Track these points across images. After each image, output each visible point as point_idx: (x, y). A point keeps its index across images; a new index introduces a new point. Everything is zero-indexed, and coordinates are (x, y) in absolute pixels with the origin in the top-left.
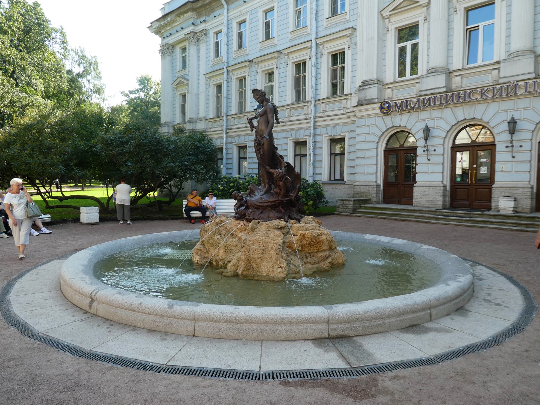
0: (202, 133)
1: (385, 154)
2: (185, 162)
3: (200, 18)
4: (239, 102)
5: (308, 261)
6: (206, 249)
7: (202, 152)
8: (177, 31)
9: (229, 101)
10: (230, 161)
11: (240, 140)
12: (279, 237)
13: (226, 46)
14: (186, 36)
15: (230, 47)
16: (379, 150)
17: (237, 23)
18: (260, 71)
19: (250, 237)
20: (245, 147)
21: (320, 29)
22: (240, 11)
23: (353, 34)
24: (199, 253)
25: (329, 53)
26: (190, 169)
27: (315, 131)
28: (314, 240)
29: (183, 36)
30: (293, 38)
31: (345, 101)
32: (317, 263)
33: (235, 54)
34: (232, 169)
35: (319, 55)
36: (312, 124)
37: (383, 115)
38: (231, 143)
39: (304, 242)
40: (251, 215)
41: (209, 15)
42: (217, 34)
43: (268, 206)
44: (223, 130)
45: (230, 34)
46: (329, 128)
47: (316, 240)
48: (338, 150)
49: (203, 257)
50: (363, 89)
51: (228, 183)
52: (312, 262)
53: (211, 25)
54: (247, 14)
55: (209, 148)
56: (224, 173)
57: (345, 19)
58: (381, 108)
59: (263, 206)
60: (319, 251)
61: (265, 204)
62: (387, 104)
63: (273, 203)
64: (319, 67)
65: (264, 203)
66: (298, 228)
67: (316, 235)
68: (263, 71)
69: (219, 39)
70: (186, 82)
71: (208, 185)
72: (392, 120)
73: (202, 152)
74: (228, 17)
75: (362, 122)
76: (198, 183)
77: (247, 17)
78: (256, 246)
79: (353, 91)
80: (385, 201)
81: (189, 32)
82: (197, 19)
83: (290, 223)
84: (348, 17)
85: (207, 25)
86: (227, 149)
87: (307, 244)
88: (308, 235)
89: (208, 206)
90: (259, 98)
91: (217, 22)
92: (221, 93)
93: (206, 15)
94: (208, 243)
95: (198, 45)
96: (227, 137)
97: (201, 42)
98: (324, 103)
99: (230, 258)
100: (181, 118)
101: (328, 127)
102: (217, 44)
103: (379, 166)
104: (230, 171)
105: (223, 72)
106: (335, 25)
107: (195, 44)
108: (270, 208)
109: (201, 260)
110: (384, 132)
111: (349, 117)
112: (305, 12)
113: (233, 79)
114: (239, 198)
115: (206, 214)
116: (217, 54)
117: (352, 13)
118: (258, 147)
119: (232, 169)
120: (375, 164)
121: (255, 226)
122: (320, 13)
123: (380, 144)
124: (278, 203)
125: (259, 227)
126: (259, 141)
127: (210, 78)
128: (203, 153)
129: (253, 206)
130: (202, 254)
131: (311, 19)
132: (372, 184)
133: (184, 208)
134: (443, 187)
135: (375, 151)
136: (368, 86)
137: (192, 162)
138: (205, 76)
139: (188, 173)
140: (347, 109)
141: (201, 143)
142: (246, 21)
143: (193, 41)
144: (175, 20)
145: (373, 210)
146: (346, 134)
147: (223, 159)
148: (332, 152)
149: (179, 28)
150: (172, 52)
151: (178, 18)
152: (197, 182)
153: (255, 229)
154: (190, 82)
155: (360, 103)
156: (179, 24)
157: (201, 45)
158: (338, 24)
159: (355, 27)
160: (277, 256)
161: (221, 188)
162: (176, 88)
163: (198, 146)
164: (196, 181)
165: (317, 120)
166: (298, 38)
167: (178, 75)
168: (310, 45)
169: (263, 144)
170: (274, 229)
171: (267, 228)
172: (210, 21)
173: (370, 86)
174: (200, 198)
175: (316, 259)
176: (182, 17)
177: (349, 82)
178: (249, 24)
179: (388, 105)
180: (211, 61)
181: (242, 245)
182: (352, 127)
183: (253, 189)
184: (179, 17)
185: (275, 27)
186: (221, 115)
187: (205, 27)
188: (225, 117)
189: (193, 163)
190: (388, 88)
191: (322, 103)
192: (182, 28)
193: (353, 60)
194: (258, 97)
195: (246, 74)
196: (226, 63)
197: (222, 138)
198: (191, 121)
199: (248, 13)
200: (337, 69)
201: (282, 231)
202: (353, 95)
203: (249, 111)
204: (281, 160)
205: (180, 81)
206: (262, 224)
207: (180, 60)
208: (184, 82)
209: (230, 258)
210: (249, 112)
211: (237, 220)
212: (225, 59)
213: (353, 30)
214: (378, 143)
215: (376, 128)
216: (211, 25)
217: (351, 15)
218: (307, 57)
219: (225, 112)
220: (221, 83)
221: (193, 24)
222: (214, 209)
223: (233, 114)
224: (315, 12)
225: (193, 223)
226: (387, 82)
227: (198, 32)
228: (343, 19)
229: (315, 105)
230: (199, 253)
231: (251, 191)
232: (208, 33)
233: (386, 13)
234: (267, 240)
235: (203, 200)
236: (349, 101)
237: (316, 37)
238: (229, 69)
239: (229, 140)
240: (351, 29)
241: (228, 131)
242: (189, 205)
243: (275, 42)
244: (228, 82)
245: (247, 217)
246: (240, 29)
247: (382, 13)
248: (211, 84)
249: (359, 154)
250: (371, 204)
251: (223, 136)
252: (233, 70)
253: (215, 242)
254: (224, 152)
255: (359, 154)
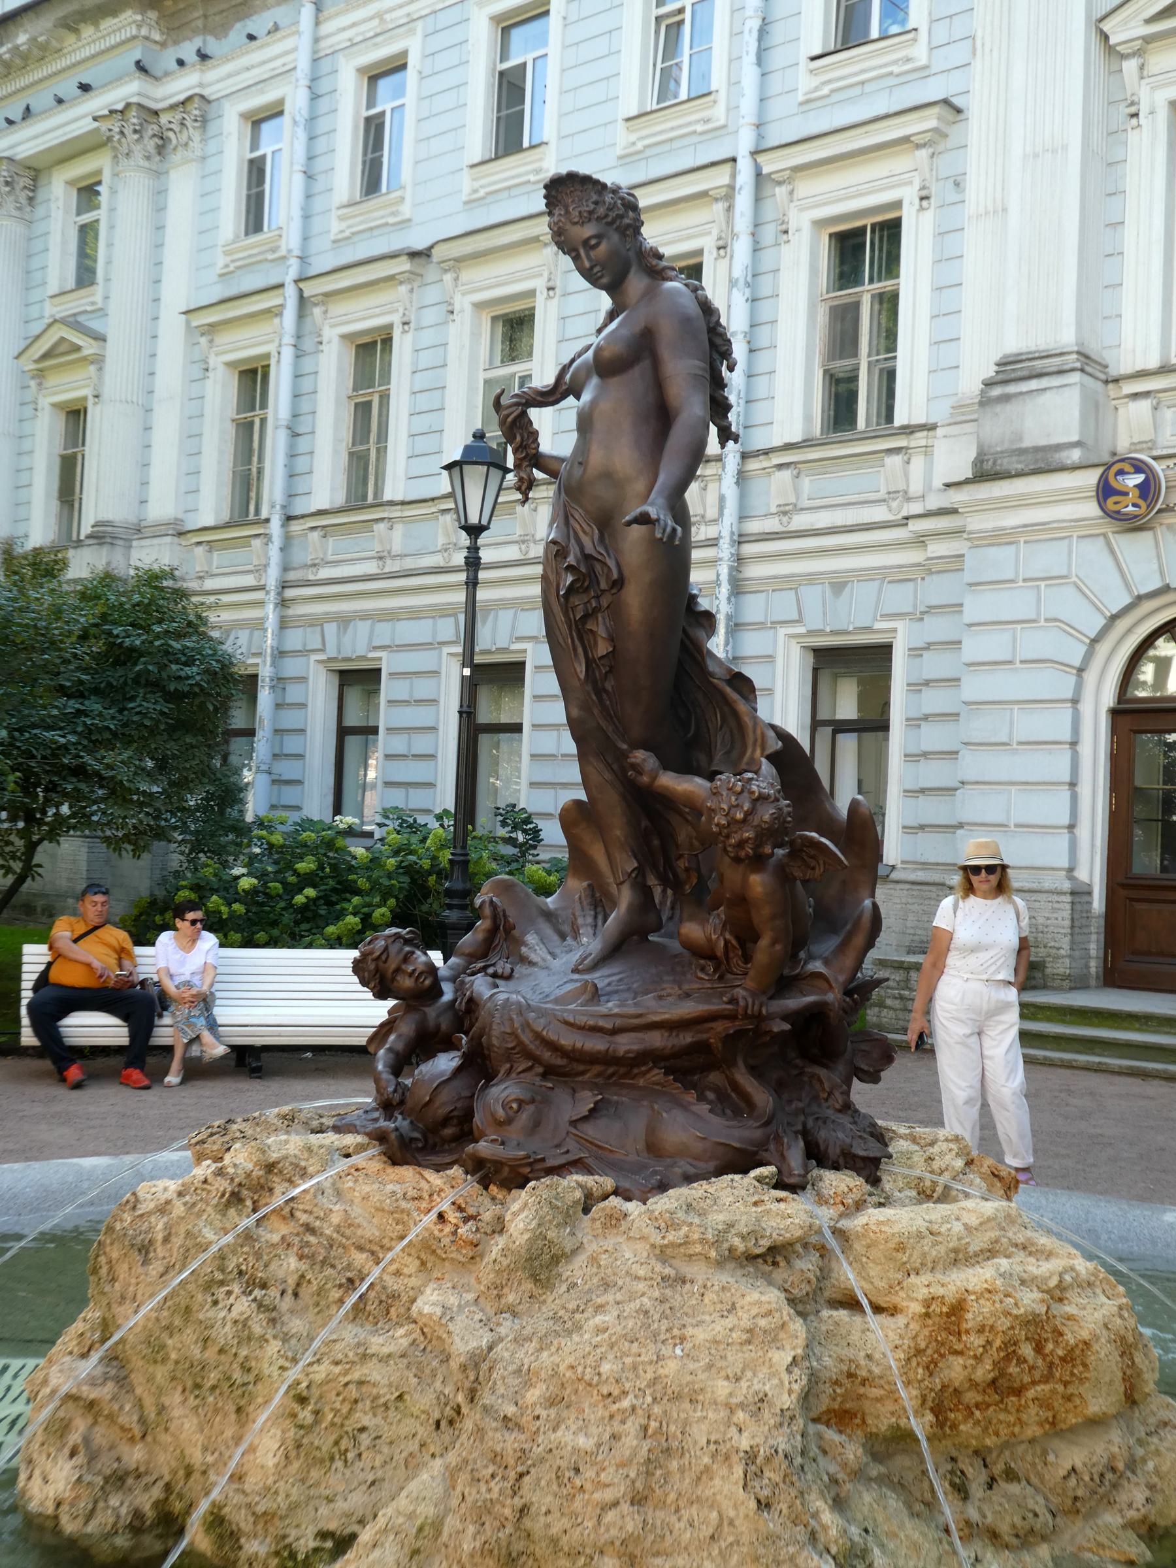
0: (152, 579)
1: (1114, 730)
2: (49, 728)
3: (176, 43)
4: (351, 454)
5: (973, 1515)
6: (139, 1404)
7: (149, 684)
8: (60, 101)
9: (303, 444)
10: (292, 744)
11: (347, 639)
12: (773, 1338)
13: (298, 179)
14: (104, 126)
15: (318, 186)
16: (1086, 707)
17: (361, 71)
18: (463, 303)
19: (520, 1340)
20: (373, 676)
21: (777, 108)
22: (379, 15)
23: (945, 136)
24: (80, 1425)
25: (819, 224)
26: (80, 771)
27: (737, 608)
28: (1027, 1350)
29: (88, 125)
30: (639, 146)
31: (896, 460)
32: (1044, 1538)
33: (341, 219)
34: (299, 782)
35: (769, 233)
36: (724, 571)
37: (1108, 527)
38: (305, 652)
39: (955, 1370)
40: (514, 1132)
41: (221, 31)
42: (257, 120)
43: (647, 1057)
44: (262, 588)
45: (322, 125)
46: (812, 596)
47: (1039, 1349)
48: (847, 708)
49: (106, 1464)
50: (1006, 398)
51: (284, 855)
52: (1004, 1528)
53: (229, 76)
54: (412, 32)
55: (189, 663)
56: (254, 806)
57: (908, 60)
58: (1106, 491)
59: (606, 1059)
60: (1055, 1428)
61: (626, 1044)
62: (1138, 470)
63: (687, 1038)
64: (765, 290)
65: (614, 1032)
66: (901, 1248)
67: (1030, 1300)
68: (479, 306)
69: (265, 149)
70: (89, 348)
71: (176, 860)
72: (1159, 557)
73: (149, 684)
74: (316, 40)
75: (1000, 562)
76: (118, 850)
77: (414, 46)
78: (584, 1429)
79: (939, 414)
80: (1112, 978)
81: (120, 107)
82: (163, 45)
83: (821, 1200)
84: (920, 52)
85: (212, 75)
86: (280, 683)
87: (973, 1384)
88: (986, 1307)
89: (170, 987)
90: (599, 237)
91: (264, 63)
92: (264, 405)
93: (206, 30)
94: (156, 1352)
95: (158, 174)
96: (283, 624)
97: (176, 158)
98: (786, 465)
99: (341, 1505)
100: (53, 521)
101: (803, 590)
102: (256, 171)
103: (1084, 790)
104: (289, 795)
105: (277, 301)
106: (857, 91)
107: (146, 164)
108: (657, 1075)
109: (83, 1505)
110: (1114, 618)
111: (920, 540)
112: (703, 32)
113: (325, 339)
114: (407, 983)
115: (157, 1031)
116: (254, 217)
117: (941, 36)
118: (576, 600)
119: (299, 782)
120: (1067, 778)
121: (561, 1237)
122: (778, 33)
123: (1091, 677)
124: (731, 1040)
125: (592, 1247)
126: (587, 557)
127: (212, 329)
128: (156, 686)
129: (529, 1055)
130: (102, 1435)
131: (734, 60)
132: (1047, 885)
133: (27, 995)
134: (1073, 893)
135: (1067, 714)
136: (1034, 384)
137: (89, 731)
138: (188, 323)
139: (65, 795)
140: (908, 499)
141: (147, 629)
142: (403, 67)
143: (137, 148)
144: (54, 43)
145: (1063, 1022)
146: (899, 625)
147: (260, 734)
148: (823, 715)
149: (67, 87)
150: (31, 199)
151: (71, 39)
152: (114, 844)
153: (556, 1260)
154: (113, 350)
155: (988, 466)
156: (74, 65)
157: (173, 175)
158: (868, 88)
159: (956, 101)
160: (771, 1523)
161: (246, 883)
162: (40, 374)
163: (132, 649)
164: (107, 840)
165: (749, 549)
166: (666, 147)
167: (51, 310)
168: (726, 180)
169: (619, 583)
170: (720, 1264)
171: (663, 1254)
172: (227, 59)
173: (1044, 382)
174: (120, 936)
175: (1038, 1504)
176: (88, 31)
177: (922, 366)
178: (422, 77)
179: (1140, 478)
180: (220, 250)
181: (442, 1400)
182: (938, 590)
183: (513, 915)
184: (76, 31)
185: (551, 94)
186: (257, 511)
187: (201, 85)
188: (275, 527)
189: (95, 740)
190: (1136, 396)
191: (780, 467)
192: (85, 88)
193: (945, 259)
194: (588, 231)
195: (396, 318)
196: (294, 264)
197: (258, 625)
198: (103, 536)
199: (420, 25)
200: (856, 306)
201: (780, 1275)
202: (940, 432)
203: (399, 497)
204: (742, 707)
205: (62, 339)
206: (615, 1220)
207: (64, 242)
208: (78, 348)
209: (341, 1505)
210: (403, 503)
211: (395, 1160)
212: (292, 241)
213: (949, 115)
214: (1081, 670)
215: (1070, 591)
216: (229, 76)
217: (934, 44)
218: (708, 243)
219: (279, 497)
220: (267, 356)
221: (140, 67)
222: (205, 1002)
223: (321, 513)
224: (755, 24)
225: (78, 1086)
226: (1125, 368)
227: (164, 110)
228: (895, 62)
229: (742, 477)
230: (80, 1425)
231: (493, 932)
232: (211, 116)
233: (1123, 30)
234: (670, 1368)
235: (139, 950)
236: (918, 462)
237: (757, 145)
238: (309, 289)
239: (294, 639)
240: (936, 110)
241: (290, 593)
242: (55, 976)
243: (545, 165)
244: (299, 354)
245: (483, 1148)
246: (371, 103)
247: (1106, 27)
248: (216, 361)
249: (979, 727)
250: (1045, 987)
251: (263, 620)
252: (327, 295)
253: (211, 1354)
254: (265, 697)
255: (979, 727)
